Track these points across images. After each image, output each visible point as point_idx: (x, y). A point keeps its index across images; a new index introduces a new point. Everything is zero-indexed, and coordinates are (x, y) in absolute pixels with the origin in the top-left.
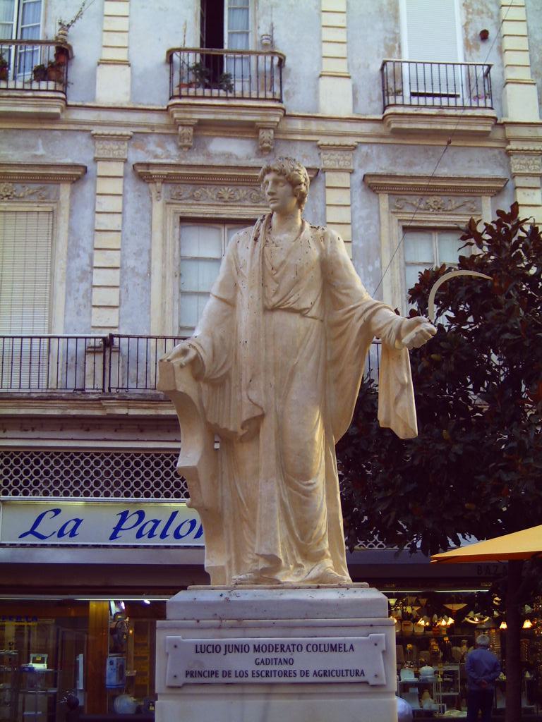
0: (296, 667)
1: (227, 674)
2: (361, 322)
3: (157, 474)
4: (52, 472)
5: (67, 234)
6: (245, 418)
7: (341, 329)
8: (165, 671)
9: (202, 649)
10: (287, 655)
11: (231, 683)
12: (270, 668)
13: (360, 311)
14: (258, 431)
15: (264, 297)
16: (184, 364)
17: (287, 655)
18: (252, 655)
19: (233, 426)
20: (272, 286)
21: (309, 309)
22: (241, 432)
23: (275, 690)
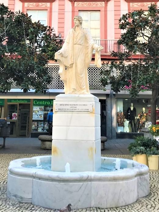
0: (77, 108)
1: (65, 109)
2: (91, 46)
3: (92, 74)
4: (93, 72)
5: (37, 162)
6: (70, 64)
7: (88, 47)
8: (55, 108)
9: (61, 105)
10: (75, 106)
11: (65, 111)
12: (72, 108)
13: (91, 44)
14: (72, 66)
15: (73, 42)
16: (54, 61)
17: (75, 106)
18: (70, 106)
19: (68, 65)
20: (75, 40)
21: (82, 44)
22: (70, 66)
23: (74, 112)
